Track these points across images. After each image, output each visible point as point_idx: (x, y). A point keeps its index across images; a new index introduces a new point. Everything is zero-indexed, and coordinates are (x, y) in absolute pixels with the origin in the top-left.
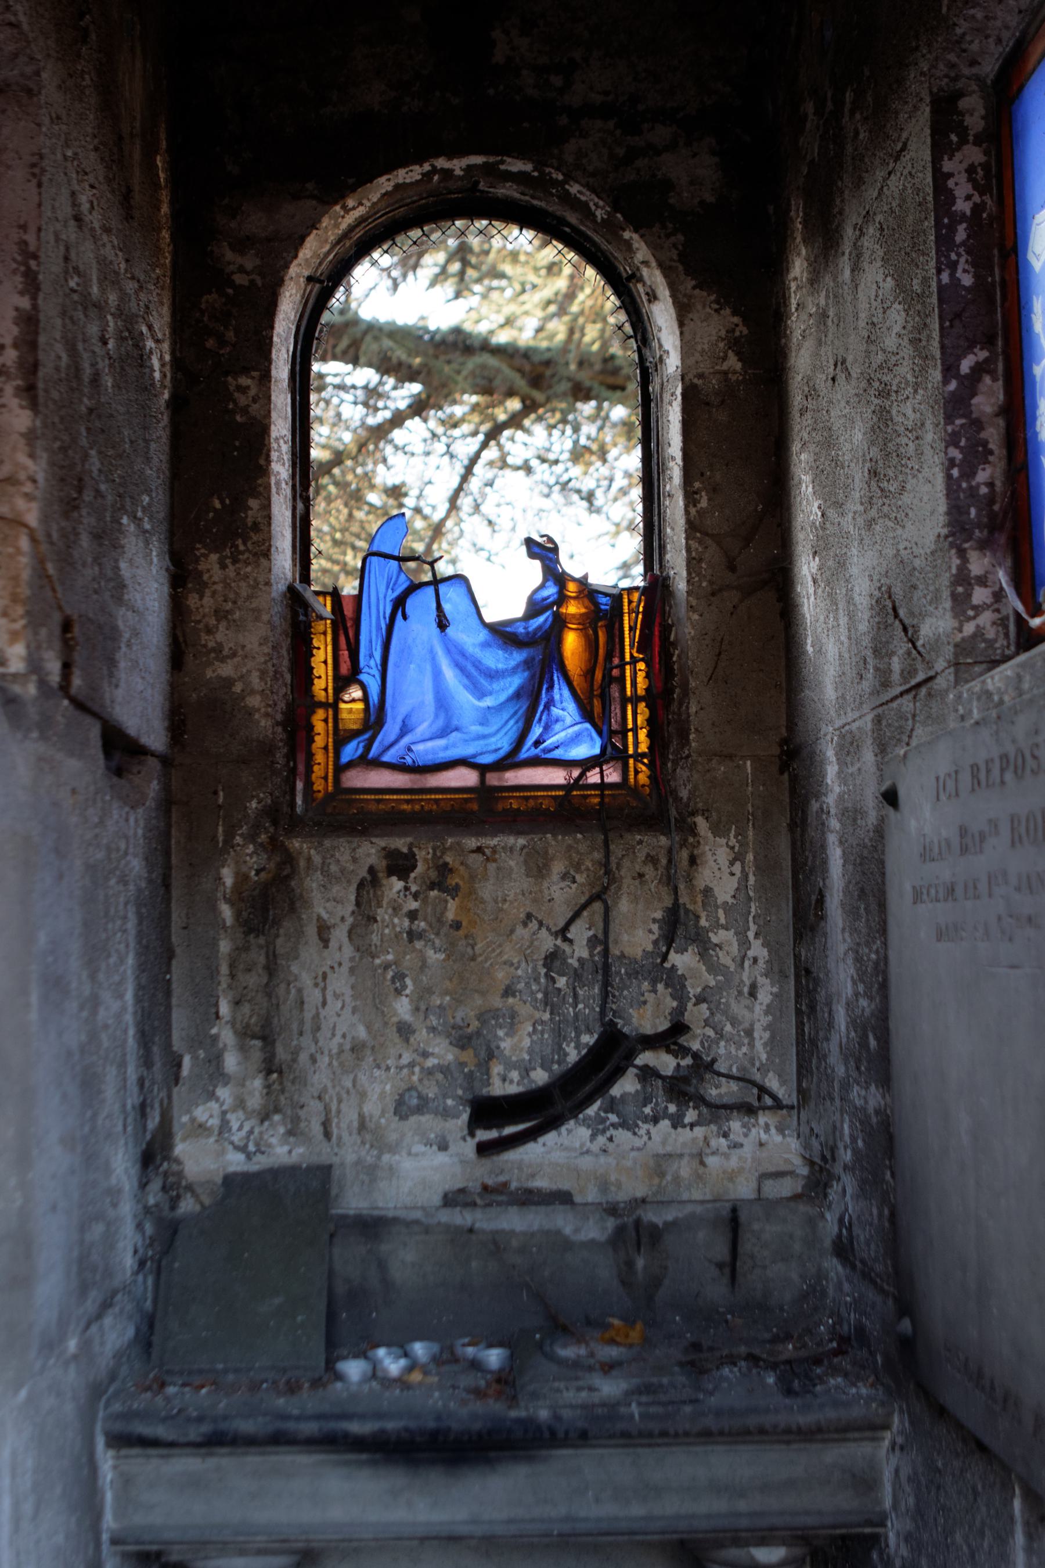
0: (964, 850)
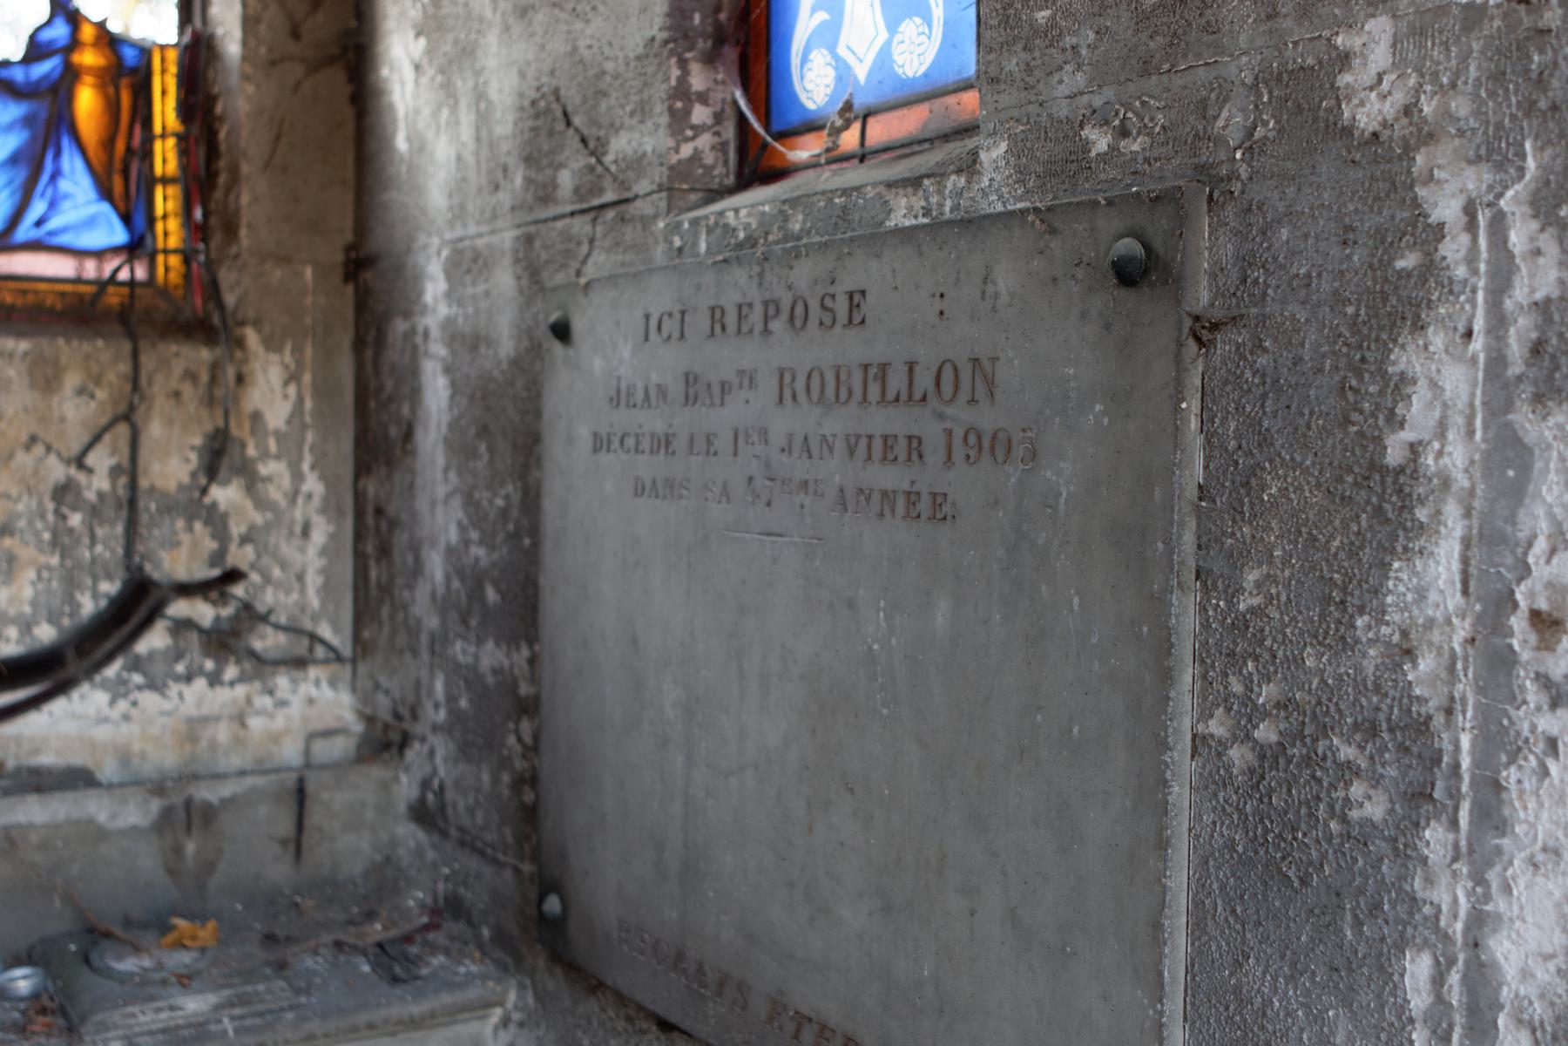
0: (689, 399)
